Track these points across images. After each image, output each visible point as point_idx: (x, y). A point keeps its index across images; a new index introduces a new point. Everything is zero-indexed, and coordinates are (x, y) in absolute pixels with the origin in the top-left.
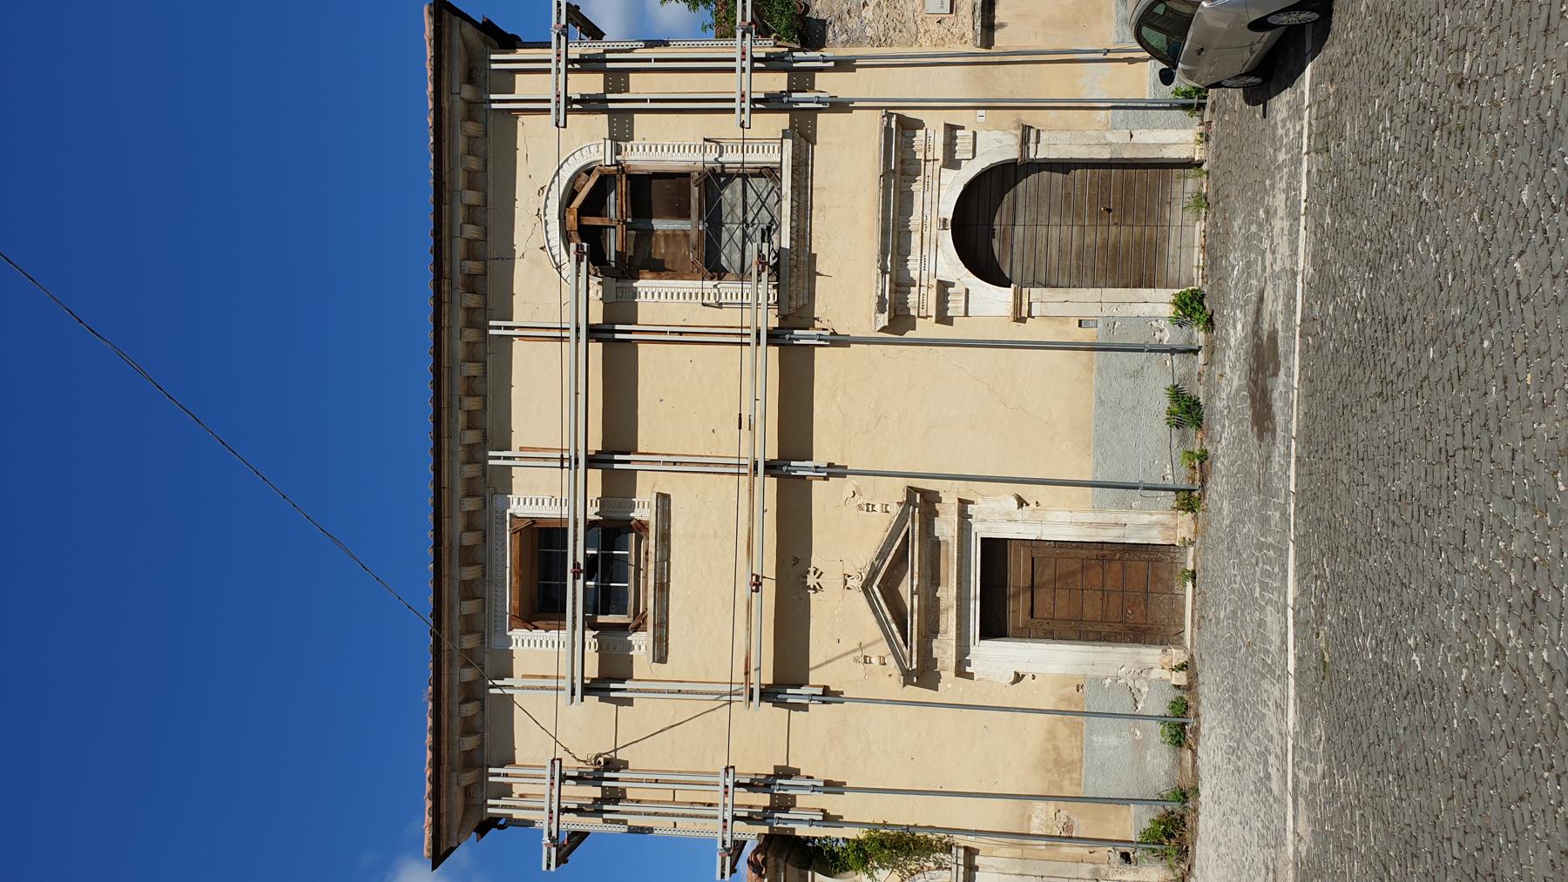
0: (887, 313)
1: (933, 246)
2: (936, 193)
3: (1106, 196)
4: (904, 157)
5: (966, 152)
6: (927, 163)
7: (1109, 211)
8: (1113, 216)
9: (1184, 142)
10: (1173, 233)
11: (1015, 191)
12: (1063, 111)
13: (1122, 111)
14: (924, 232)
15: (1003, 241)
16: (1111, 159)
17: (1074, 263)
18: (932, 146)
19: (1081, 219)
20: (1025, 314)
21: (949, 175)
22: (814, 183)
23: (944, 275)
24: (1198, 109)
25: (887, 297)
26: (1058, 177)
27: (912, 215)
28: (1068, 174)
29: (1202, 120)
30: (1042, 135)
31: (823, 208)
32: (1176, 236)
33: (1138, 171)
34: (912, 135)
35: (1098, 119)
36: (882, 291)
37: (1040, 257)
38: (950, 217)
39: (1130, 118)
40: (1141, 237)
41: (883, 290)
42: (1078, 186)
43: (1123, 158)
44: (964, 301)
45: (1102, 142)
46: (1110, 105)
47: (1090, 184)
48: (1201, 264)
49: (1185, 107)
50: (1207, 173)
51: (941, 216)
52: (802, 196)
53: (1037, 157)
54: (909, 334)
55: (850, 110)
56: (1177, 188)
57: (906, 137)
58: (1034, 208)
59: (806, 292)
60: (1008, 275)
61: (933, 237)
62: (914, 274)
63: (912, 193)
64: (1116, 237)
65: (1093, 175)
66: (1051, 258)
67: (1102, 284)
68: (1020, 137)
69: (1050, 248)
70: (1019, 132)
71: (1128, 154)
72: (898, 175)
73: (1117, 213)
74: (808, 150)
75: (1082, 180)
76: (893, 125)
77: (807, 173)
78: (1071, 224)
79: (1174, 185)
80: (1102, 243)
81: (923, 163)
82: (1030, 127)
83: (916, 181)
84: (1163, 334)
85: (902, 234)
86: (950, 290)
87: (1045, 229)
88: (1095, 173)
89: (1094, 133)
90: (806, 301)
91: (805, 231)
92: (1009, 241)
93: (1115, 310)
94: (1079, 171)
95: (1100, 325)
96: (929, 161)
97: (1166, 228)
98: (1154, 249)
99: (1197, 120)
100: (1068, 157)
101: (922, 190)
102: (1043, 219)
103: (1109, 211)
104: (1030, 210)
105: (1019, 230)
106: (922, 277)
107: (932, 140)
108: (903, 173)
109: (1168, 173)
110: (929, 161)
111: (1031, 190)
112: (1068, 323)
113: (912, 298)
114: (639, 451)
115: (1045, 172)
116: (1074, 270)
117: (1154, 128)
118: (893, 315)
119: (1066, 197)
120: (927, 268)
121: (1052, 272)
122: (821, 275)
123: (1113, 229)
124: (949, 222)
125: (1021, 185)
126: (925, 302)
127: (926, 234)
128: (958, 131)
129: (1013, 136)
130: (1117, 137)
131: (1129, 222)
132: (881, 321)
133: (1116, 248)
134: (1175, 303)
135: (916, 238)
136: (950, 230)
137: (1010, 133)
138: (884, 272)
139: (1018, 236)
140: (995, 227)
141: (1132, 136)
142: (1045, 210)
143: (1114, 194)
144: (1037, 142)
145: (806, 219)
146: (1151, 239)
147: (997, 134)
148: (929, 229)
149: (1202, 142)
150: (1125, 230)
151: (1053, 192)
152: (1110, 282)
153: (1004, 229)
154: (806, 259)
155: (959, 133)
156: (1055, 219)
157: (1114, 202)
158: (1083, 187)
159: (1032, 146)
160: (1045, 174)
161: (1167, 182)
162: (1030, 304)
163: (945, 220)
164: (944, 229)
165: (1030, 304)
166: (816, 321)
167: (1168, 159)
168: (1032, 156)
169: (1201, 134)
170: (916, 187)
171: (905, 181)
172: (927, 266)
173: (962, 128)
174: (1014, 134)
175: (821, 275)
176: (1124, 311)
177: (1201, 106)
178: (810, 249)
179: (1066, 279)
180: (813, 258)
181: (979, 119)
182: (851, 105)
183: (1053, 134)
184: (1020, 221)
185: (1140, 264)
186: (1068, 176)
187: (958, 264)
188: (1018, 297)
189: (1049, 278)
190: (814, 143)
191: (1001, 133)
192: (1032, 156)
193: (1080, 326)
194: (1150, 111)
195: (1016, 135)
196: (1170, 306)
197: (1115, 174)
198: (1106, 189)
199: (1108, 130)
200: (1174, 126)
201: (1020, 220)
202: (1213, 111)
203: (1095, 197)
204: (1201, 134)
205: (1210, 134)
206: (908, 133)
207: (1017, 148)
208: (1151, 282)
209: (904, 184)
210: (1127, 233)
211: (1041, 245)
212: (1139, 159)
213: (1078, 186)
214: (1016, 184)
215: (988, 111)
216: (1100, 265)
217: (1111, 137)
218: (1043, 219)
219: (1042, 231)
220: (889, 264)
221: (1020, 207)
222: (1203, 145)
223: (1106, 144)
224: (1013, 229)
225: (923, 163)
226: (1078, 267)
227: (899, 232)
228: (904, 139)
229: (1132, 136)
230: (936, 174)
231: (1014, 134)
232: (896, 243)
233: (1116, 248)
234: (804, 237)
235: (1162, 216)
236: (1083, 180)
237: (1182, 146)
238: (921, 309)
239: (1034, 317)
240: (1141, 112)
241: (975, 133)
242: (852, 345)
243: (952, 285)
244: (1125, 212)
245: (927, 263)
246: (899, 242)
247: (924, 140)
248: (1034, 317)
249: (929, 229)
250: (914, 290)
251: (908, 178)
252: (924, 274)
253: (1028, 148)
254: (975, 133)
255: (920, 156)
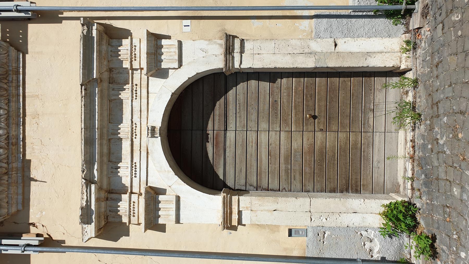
0: (93, 224)
1: (144, 154)
2: (144, 101)
3: (311, 103)
4: (112, 66)
5: (171, 61)
6: (135, 72)
7: (315, 117)
8: (319, 123)
9: (389, 50)
10: (377, 139)
11: (226, 99)
12: (267, 21)
13: (325, 20)
14: (134, 139)
15: (216, 145)
16: (316, 68)
17: (283, 167)
18: (138, 56)
19: (287, 125)
20: (235, 223)
21: (155, 83)
22: (27, 91)
23: (155, 182)
24: (404, 17)
25: (93, 207)
26: (265, 85)
27: (122, 122)
28: (274, 82)
29: (407, 28)
30: (247, 45)
31: (36, 115)
32: (380, 142)
33: (342, 79)
34: (118, 44)
35: (302, 28)
36: (87, 201)
37: (251, 160)
38: (158, 124)
39: (334, 27)
40: (346, 143)
41: (88, 202)
42: (284, 94)
43: (327, 67)
44: (174, 209)
45: (306, 51)
46: (313, 13)
47: (296, 92)
48: (410, 174)
49: (389, 15)
50: (416, 82)
51: (150, 125)
52: (13, 104)
53: (242, 66)
54: (123, 242)
55: (59, 20)
56: (379, 96)
57: (112, 46)
58: (243, 114)
59: (20, 197)
60: (221, 177)
61: (144, 145)
62: (126, 181)
63: (121, 102)
64: (322, 143)
65: (298, 83)
66: (261, 162)
67: (310, 187)
68: (224, 46)
69: (261, 152)
70: (223, 42)
71: (332, 63)
72: (105, 84)
73: (322, 119)
74: (18, 59)
75: (288, 88)
76: (94, 33)
77: (18, 81)
78: (278, 129)
79: (377, 93)
80: (309, 148)
81: (130, 71)
82: (234, 37)
83: (125, 89)
84: (372, 244)
85: (112, 141)
86: (161, 198)
87: (254, 135)
88: (300, 81)
89: (298, 43)
90: (20, 207)
91: (17, 138)
92: (222, 145)
93: (324, 220)
94: (284, 80)
95: (310, 234)
96: (137, 70)
97: (369, 134)
98: (359, 154)
99: (402, 28)
100: (272, 66)
101: (130, 98)
102: (252, 125)
103: (315, 117)
104: (240, 117)
105: (230, 135)
106: (134, 184)
107: (137, 48)
108: (111, 81)
109: (371, 80)
110: (137, 70)
111: (241, 97)
112: (278, 231)
113: (123, 206)
114: (38, 241)
115: (284, 79)
116: (283, 174)
117: (358, 37)
118: (103, 223)
119: (273, 105)
120: (138, 175)
121: (263, 176)
122: (36, 181)
123: (319, 135)
124: (157, 131)
125: (231, 93)
126: (136, 209)
127: (136, 142)
128: (163, 40)
129: (218, 46)
130: (263, 145)
131: (334, 128)
132: (89, 232)
133: (323, 152)
134: (385, 215)
135: (126, 146)
136: (159, 138)
137: (215, 42)
138: (89, 181)
139: (230, 139)
140: (208, 132)
141: (336, 45)
142: (253, 116)
143: (318, 102)
144: (242, 51)
145: (18, 125)
146: (355, 144)
147: (203, 44)
148: (138, 137)
149: (408, 51)
150: (331, 136)
151: (261, 100)
152: (318, 186)
153: (217, 135)
154: (20, 165)
155: (164, 42)
156: (264, 125)
157: (319, 108)
158: (288, 95)
159: (237, 56)
160: (253, 83)
161: (371, 90)
162: (240, 213)
163: (153, 128)
164: (153, 136)
165: (240, 213)
166: (31, 227)
167: (373, 67)
168: (237, 65)
169: (408, 42)
170: (125, 95)
171: (113, 90)
172: (138, 173)
173: (169, 37)
174: (219, 44)
175: (36, 181)
176: (331, 222)
177: (409, 12)
178: (24, 155)
179: (276, 182)
180: (27, 164)
181: (188, 29)
182: (60, 16)
183: (257, 44)
184: (231, 126)
185: (346, 168)
186: (275, 85)
187: (168, 172)
188: (227, 206)
189: (261, 179)
190: (25, 52)
191: (207, 42)
192: (237, 65)
193: (290, 235)
194: (353, 20)
195: (221, 45)
196: (380, 216)
197: (320, 83)
198: (311, 96)
199: (311, 39)
200: (377, 34)
201: (231, 126)
202: (424, 15)
203: (301, 104)
204: (408, 42)
205: (418, 41)
206: (114, 42)
207: (222, 57)
208: (357, 186)
209: (113, 92)
210: (332, 139)
211: (251, 150)
212: (344, 68)
213: (284, 94)
214: (226, 92)
215: (193, 21)
216: (308, 170)
217: (315, 46)
218: (252, 125)
219: (252, 136)
220: (96, 172)
221: (231, 114)
222: (411, 54)
223: (311, 53)
224: (225, 134)
225: (130, 71)
226: (286, 171)
227: (110, 140)
228: (110, 49)
229: (336, 45)
230: (144, 83)
231: (219, 44)
232: (105, 150)
233: (323, 152)
234: (17, 144)
235: (365, 123)
236: (289, 89)
237: (387, 55)
238: (132, 217)
239: (244, 225)
240: (345, 21)
241: (180, 43)
242: (66, 252)
243: (163, 192)
244: (329, 119)
245: (138, 170)
246: (109, 149)
247: (129, 48)
248: (244, 225)
249: (138, 137)
250: (125, 197)
251: (116, 86)
252: (136, 181)
253: (233, 57)
254: (180, 43)
255: (126, 65)
